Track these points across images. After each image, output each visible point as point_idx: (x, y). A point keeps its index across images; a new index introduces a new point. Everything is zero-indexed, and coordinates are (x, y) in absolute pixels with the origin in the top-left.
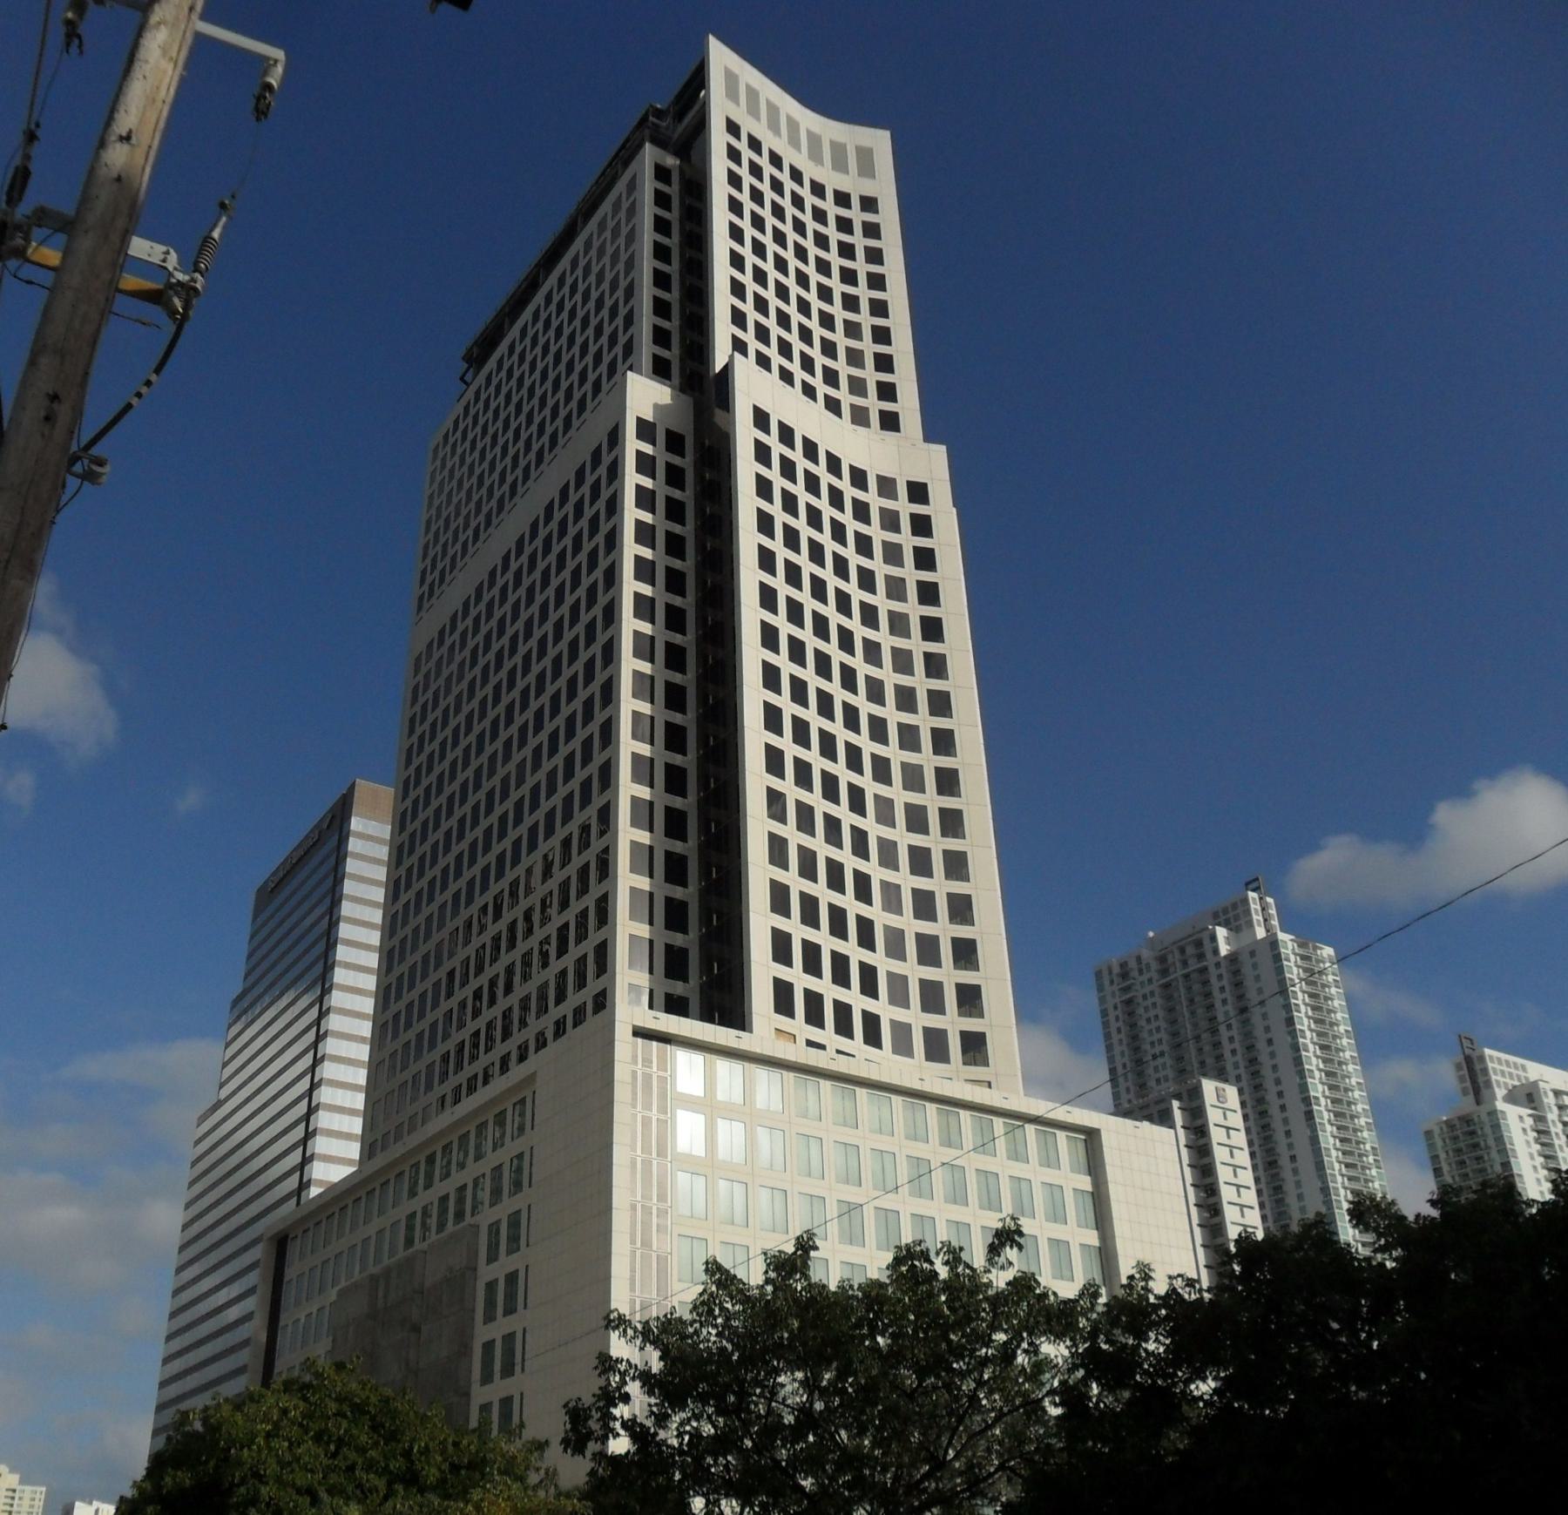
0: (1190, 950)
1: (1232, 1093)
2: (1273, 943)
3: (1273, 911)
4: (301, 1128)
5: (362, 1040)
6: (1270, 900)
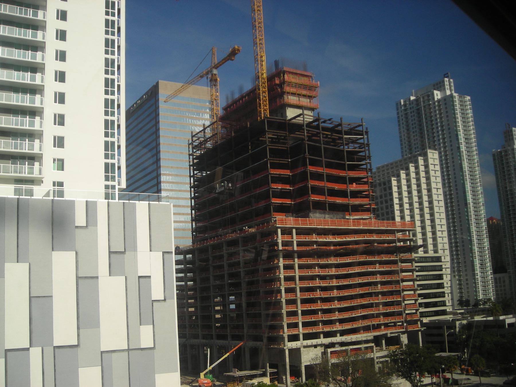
0: (426, 98)
1: (436, 155)
2: (451, 96)
3: (452, 84)
4: (154, 128)
5: (164, 182)
6: (451, 80)
